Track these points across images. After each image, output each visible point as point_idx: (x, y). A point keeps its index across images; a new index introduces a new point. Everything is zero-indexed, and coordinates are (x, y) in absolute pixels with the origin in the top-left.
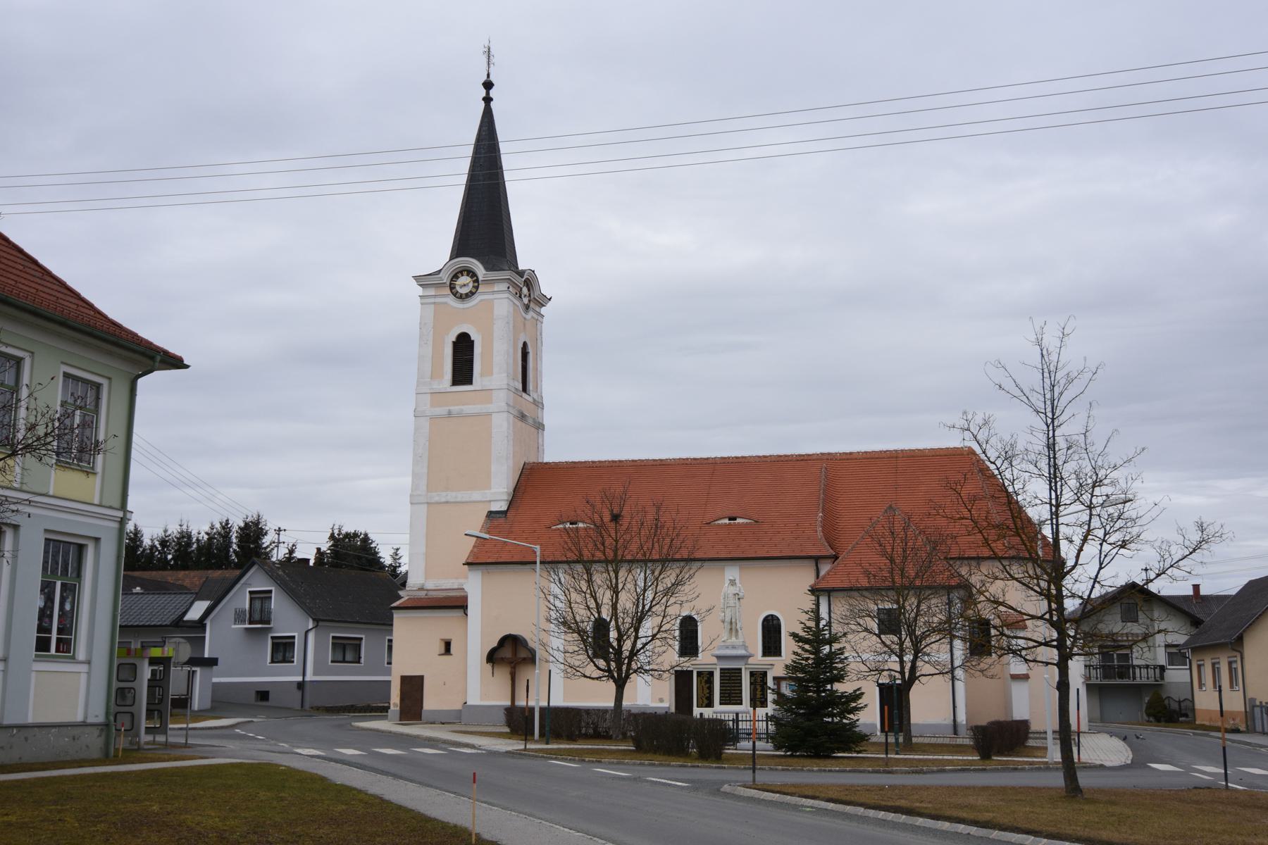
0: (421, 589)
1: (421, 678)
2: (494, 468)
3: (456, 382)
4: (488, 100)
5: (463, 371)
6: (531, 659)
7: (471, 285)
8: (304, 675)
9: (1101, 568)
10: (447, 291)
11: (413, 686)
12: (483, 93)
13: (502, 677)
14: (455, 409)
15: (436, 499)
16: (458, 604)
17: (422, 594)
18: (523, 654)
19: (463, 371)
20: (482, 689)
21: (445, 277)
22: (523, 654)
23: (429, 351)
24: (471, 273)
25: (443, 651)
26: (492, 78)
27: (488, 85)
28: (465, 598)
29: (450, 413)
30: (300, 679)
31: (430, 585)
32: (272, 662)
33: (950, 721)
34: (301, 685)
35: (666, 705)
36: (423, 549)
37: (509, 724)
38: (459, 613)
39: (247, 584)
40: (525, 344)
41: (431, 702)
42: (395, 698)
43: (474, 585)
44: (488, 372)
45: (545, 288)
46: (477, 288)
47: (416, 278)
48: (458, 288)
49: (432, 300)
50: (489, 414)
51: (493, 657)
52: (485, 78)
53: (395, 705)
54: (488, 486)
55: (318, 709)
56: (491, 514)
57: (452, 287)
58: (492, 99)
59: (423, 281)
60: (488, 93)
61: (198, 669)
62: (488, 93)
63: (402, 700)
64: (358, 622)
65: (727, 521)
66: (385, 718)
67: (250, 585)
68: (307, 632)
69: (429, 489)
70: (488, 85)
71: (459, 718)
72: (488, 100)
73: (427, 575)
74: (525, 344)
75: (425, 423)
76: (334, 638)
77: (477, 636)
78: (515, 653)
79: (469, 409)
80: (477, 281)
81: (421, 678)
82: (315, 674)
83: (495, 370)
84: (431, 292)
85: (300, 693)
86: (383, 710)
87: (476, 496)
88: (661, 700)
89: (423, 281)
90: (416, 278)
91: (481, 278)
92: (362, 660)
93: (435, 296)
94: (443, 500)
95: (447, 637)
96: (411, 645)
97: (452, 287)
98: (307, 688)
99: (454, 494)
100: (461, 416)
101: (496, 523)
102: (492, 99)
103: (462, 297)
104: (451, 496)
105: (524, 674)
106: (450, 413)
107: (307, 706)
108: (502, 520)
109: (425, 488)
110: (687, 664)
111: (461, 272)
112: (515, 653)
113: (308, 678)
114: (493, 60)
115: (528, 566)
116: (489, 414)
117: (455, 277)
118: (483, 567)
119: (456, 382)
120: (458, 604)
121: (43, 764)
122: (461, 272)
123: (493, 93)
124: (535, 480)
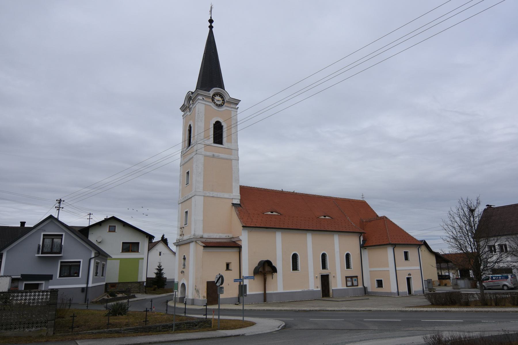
4: (211, 27)
6: (274, 270)
8: (87, 284)
12: (209, 24)
14: (216, 154)
15: (208, 194)
16: (234, 245)
25: (225, 268)
26: (212, 18)
27: (211, 21)
29: (213, 155)
30: (84, 286)
32: (60, 276)
33: (422, 289)
34: (83, 289)
36: (202, 218)
37: (429, 299)
38: (236, 250)
43: (245, 238)
46: (224, 103)
48: (215, 101)
50: (231, 160)
57: (213, 99)
58: (213, 27)
60: (211, 24)
61: (43, 282)
62: (211, 24)
65: (323, 217)
67: (45, 231)
68: (91, 259)
69: (204, 190)
70: (211, 21)
72: (211, 27)
73: (204, 231)
80: (224, 100)
81: (207, 282)
87: (226, 195)
88: (317, 287)
94: (211, 195)
97: (213, 100)
99: (216, 193)
100: (218, 158)
102: (213, 27)
104: (215, 194)
106: (213, 155)
110: (325, 272)
113: (90, 285)
120: (234, 245)
122: (217, 94)
123: (213, 25)
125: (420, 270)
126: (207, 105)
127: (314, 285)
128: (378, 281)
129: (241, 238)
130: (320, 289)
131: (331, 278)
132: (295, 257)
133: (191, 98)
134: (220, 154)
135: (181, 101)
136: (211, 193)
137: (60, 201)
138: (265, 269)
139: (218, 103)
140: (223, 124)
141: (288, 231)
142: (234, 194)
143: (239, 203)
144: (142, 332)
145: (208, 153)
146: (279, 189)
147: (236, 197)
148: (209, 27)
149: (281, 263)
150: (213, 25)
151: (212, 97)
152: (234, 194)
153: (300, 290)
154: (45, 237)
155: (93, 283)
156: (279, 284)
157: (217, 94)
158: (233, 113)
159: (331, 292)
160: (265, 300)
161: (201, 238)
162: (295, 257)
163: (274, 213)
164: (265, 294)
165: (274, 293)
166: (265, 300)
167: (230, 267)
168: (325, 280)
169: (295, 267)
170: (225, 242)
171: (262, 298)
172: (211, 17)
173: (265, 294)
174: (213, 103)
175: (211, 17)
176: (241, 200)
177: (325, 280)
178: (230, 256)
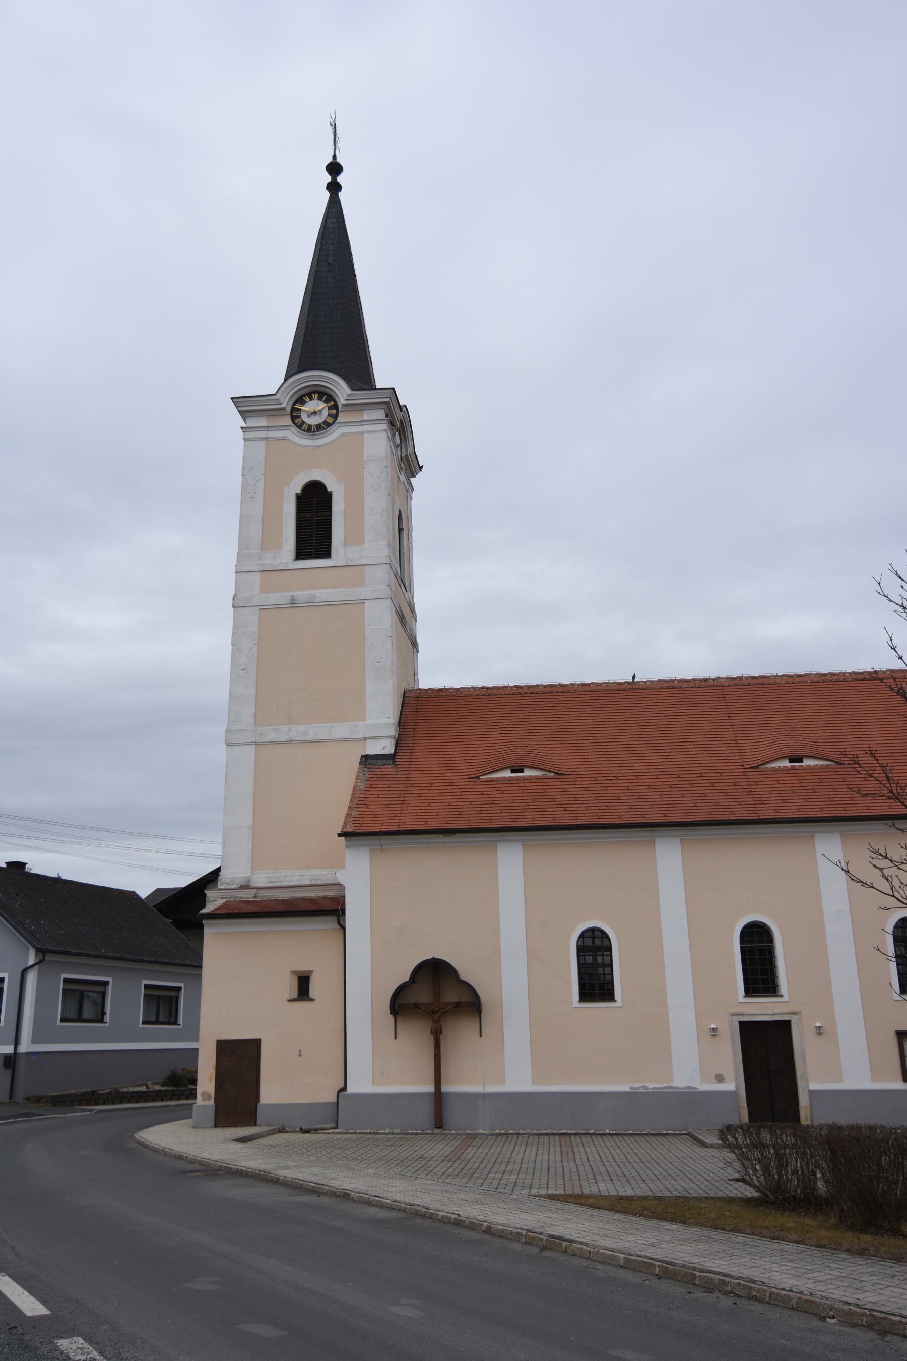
0: (246, 887)
1: (255, 1044)
2: (370, 686)
3: (301, 554)
4: (334, 188)
6: (471, 1004)
7: (325, 413)
8: (17, 1043)
10: (288, 421)
11: (240, 1060)
12: (329, 179)
13: (414, 1041)
14: (302, 595)
15: (272, 736)
16: (330, 909)
17: (248, 895)
18: (451, 996)
20: (380, 1064)
21: (286, 403)
22: (451, 996)
23: (257, 508)
24: (326, 396)
26: (339, 160)
27: (334, 169)
28: (341, 900)
30: (9, 1049)
31: (261, 879)
34: (10, 1061)
36: (248, 819)
38: (327, 924)
40: (400, 511)
41: (274, 1090)
42: (206, 1082)
43: (357, 875)
44: (355, 538)
46: (335, 417)
47: (232, 398)
48: (304, 417)
49: (263, 434)
50: (361, 602)
51: (401, 1005)
52: (330, 160)
53: (206, 1096)
54: (361, 715)
55: (38, 1100)
56: (367, 760)
57: (295, 415)
59: (247, 406)
63: (219, 1085)
64: (105, 957)
65: (786, 763)
66: (185, 1113)
68: (24, 972)
69: (259, 720)
70: (334, 169)
71: (337, 1117)
72: (334, 188)
73: (256, 862)
74: (400, 511)
75: (252, 617)
76: (66, 981)
77: (367, 963)
78: (437, 992)
80: (335, 407)
81: (255, 1044)
82: (35, 1041)
83: (369, 536)
84: (262, 422)
85: (7, 1074)
87: (340, 731)
88: (720, 1079)
89: (247, 406)
90: (232, 398)
91: (341, 401)
92: (107, 1018)
93: (268, 428)
94: (284, 738)
95: (303, 967)
96: (236, 987)
97: (295, 415)
98: (22, 1066)
99: (301, 728)
100: (311, 605)
101: (379, 772)
103: (324, 427)
104: (297, 732)
105: (461, 1036)
106: (293, 603)
107: (20, 1095)
108: (389, 769)
109: (251, 719)
110: (763, 1009)
111: (310, 395)
112: (437, 992)
113: (24, 1048)
114: (339, 145)
116: (361, 602)
117: (301, 400)
118: (375, 840)
119: (301, 554)
124: (422, 711)
126: (277, 439)
127: (701, 1064)
128: (608, 995)
129: (342, 877)
130: (733, 1082)
131: (803, 1042)
136: (285, 728)
138: (435, 998)
139: (314, 421)
141: (441, 838)
142: (369, 722)
143: (389, 749)
144: (220, 1169)
145: (275, 598)
146: (623, 676)
147: (378, 727)
150: (340, 179)
151: (293, 409)
152: (369, 722)
153: (625, 1088)
159: (804, 1100)
160: (439, 1121)
161: (242, 887)
163: (528, 773)
164: (438, 1096)
165: (484, 1096)
166: (439, 1121)
167: (315, 988)
168: (767, 1051)
169: (596, 984)
170: (325, 899)
171: (427, 1112)
172: (334, 157)
173: (438, 1096)
174: (294, 429)
175: (334, 157)
176: (398, 743)
177: (767, 1051)
178: (301, 945)
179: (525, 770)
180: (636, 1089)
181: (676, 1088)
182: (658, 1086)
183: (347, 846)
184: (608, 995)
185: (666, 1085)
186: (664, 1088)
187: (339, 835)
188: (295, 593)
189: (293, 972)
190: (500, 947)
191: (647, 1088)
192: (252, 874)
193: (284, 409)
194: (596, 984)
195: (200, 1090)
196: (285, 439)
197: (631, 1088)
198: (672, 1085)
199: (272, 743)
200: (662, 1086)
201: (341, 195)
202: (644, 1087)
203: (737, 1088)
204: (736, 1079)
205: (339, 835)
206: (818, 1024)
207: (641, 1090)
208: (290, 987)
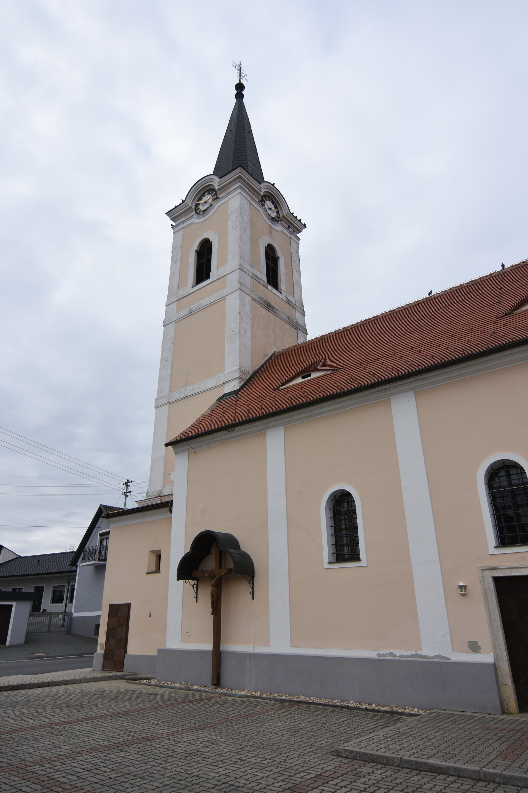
1: (128, 606)
2: (227, 349)
4: (239, 96)
5: (203, 271)
6: (243, 569)
9: (37, 790)
14: (194, 307)
19: (203, 271)
27: (240, 87)
35: (486, 657)
39: (100, 528)
41: (137, 645)
44: (223, 262)
45: (296, 206)
50: (223, 298)
61: (14, 604)
70: (240, 87)
72: (239, 96)
75: (171, 327)
79: (205, 302)
81: (128, 606)
86: (85, 656)
88: (474, 647)
94: (183, 396)
99: (191, 387)
104: (189, 390)
105: (238, 597)
115: (485, 568)
121: (13, 686)
125: (282, 222)
130: (490, 650)
132: (342, 508)
133: (203, 190)
134: (202, 302)
135: (178, 195)
137: (127, 484)
140: (279, 253)
148: (242, 96)
149: (283, 538)
153: (371, 654)
154: (103, 538)
155: (12, 605)
156: (273, 625)
157: (269, 197)
158: (293, 244)
162: (342, 508)
165: (251, 656)
169: (345, 547)
173: (217, 654)
179: (311, 375)
180: (383, 655)
181: (425, 657)
182: (406, 653)
183: (176, 453)
184: (355, 557)
185: (414, 653)
186: (412, 656)
187: (167, 445)
188: (191, 307)
189: (152, 552)
190: (267, 518)
191: (395, 656)
192: (163, 488)
193: (191, 208)
194: (345, 547)
195: (99, 642)
196: (192, 223)
197: (378, 654)
198: (420, 653)
199: (177, 401)
200: (409, 653)
201: (244, 100)
202: (391, 654)
203: (496, 658)
204: (495, 648)
205: (167, 445)
206: (461, 584)
207: (388, 658)
208: (145, 561)
